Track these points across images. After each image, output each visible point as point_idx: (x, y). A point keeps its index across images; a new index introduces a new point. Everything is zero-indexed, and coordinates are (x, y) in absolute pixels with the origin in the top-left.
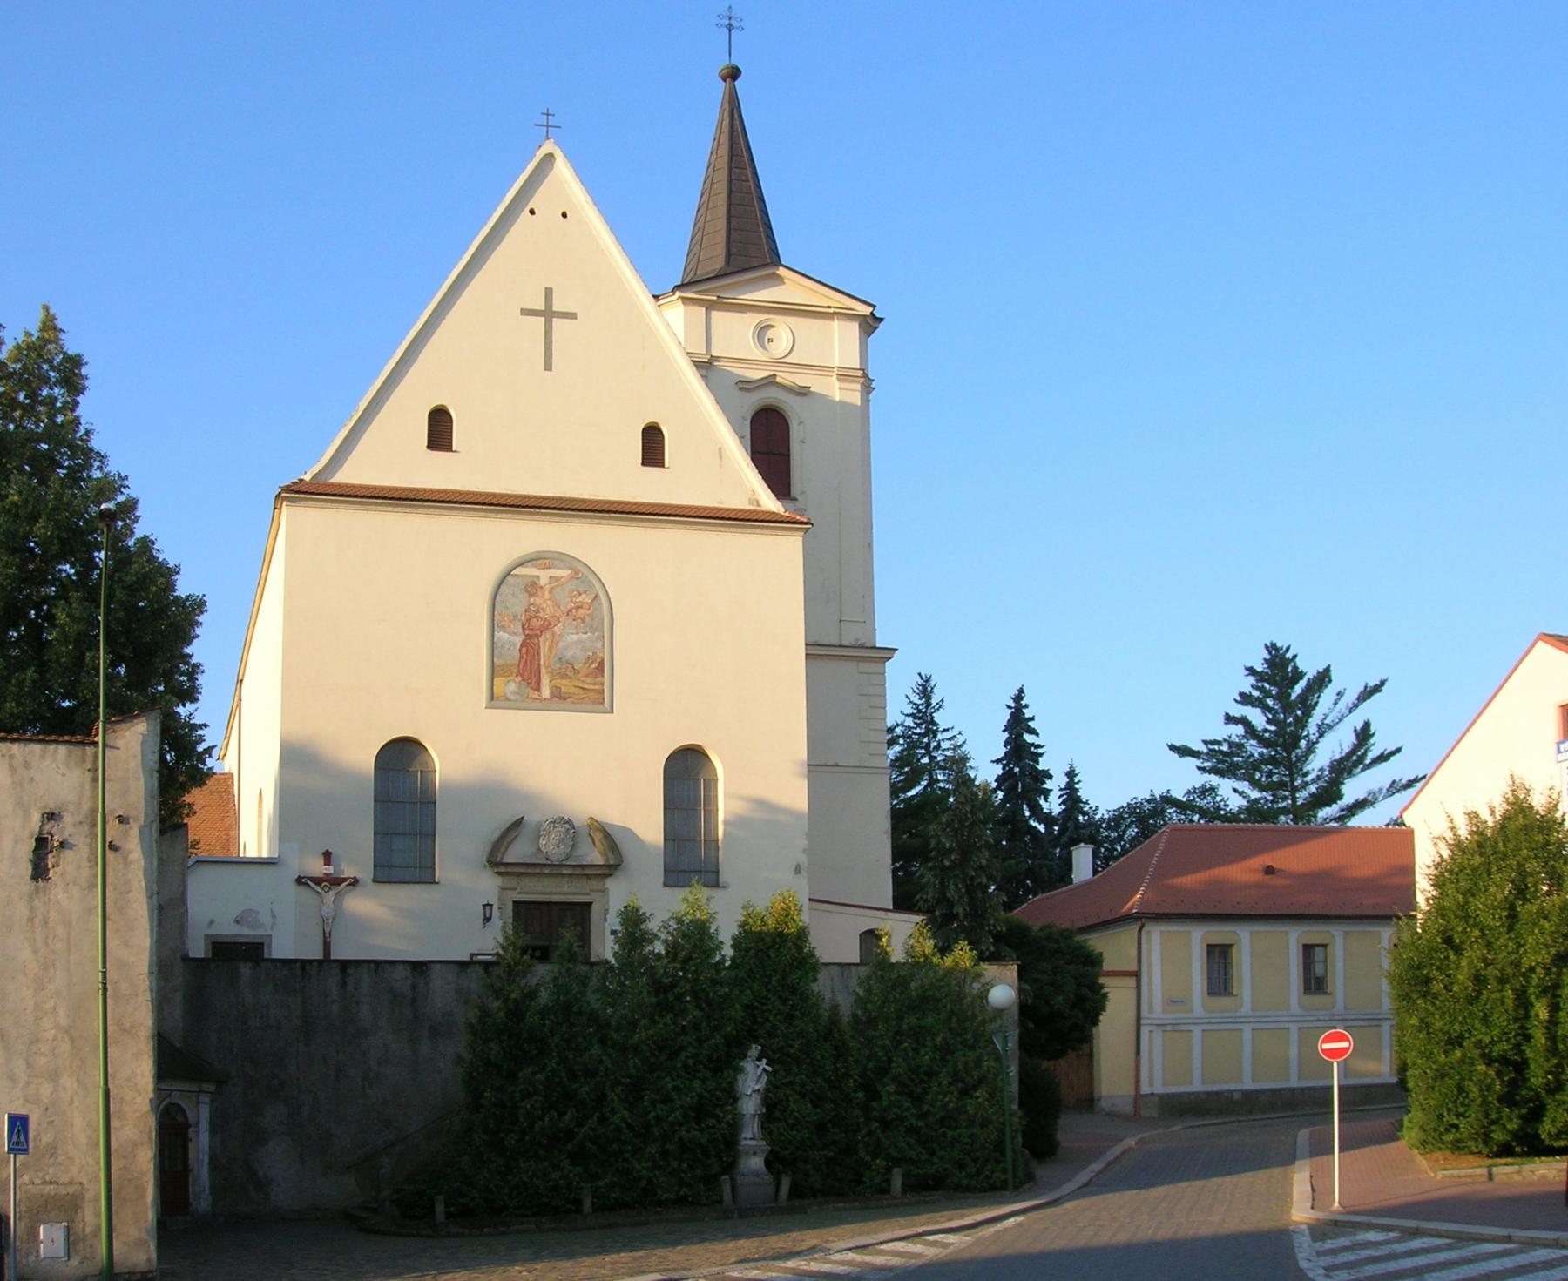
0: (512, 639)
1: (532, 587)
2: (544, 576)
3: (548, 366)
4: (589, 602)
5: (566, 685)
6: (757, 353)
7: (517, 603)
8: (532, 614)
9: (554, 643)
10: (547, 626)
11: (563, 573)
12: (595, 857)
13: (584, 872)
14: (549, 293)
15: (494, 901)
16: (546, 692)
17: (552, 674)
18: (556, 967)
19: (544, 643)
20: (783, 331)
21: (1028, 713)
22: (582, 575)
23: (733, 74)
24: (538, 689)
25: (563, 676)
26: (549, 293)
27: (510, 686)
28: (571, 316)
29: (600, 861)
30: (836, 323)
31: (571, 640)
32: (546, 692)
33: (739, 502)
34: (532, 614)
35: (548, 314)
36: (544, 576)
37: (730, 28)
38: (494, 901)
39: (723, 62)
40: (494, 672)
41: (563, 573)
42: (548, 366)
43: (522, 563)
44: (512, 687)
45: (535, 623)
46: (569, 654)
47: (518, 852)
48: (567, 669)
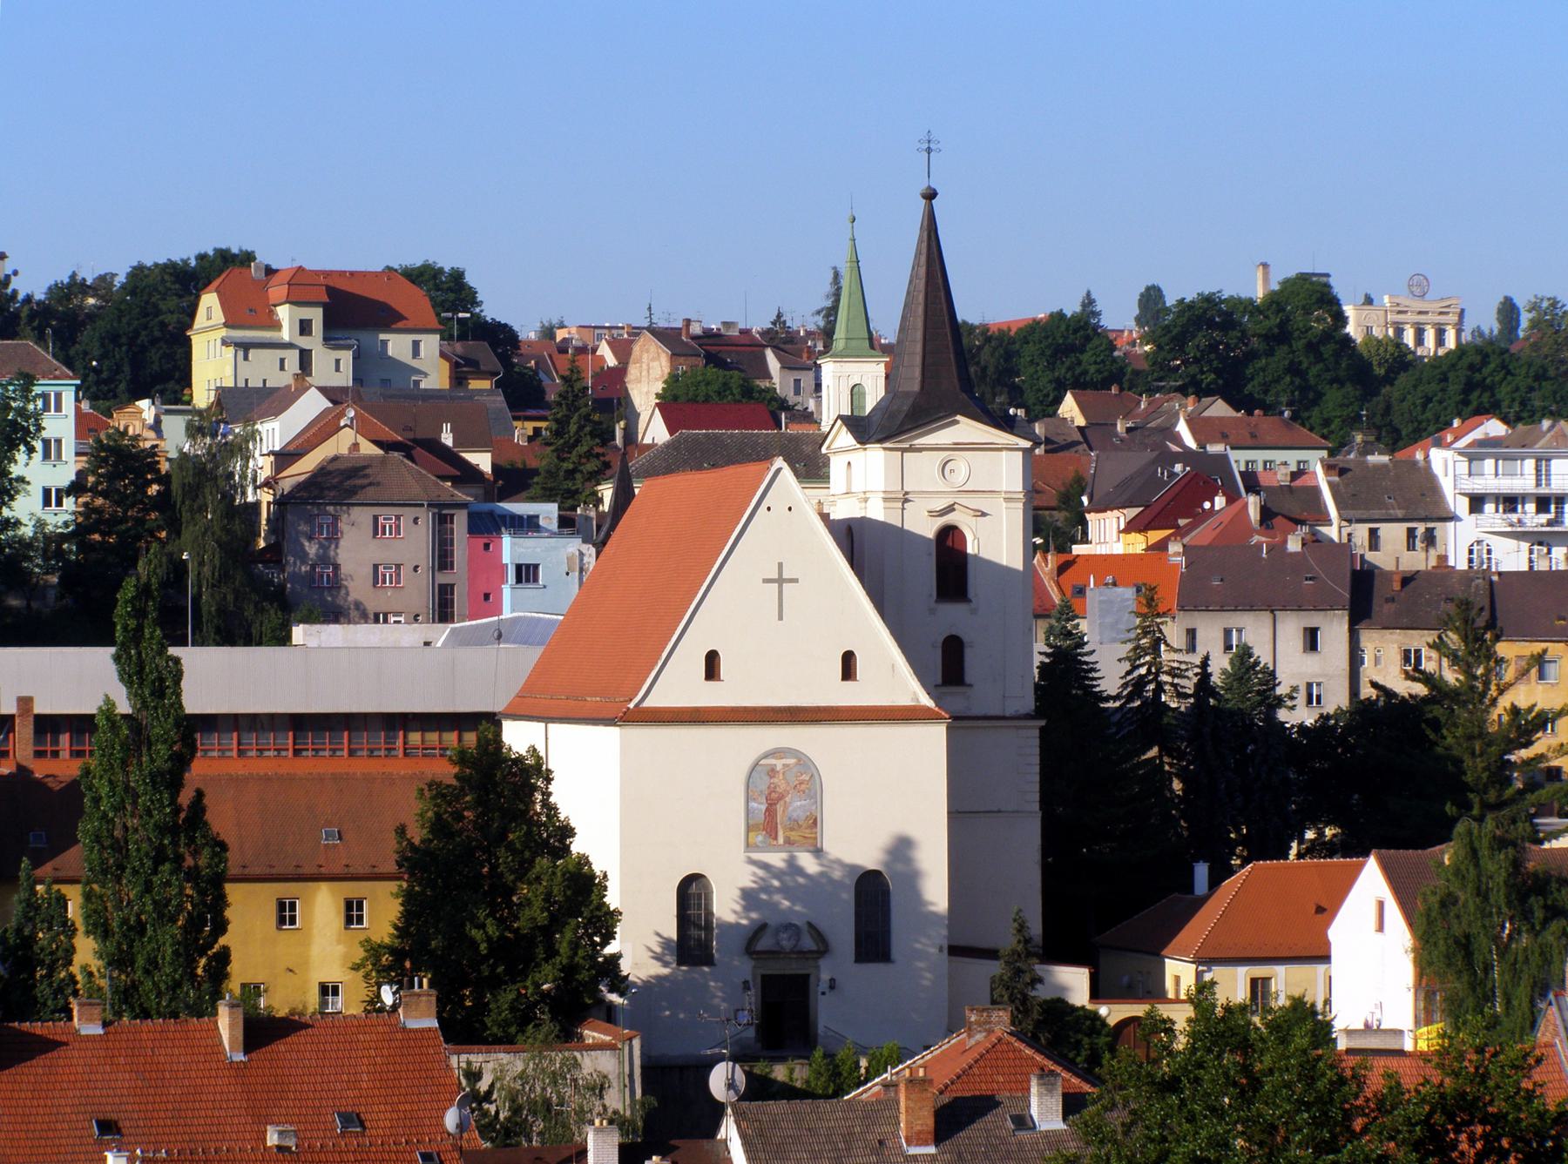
0: (760, 807)
1: (772, 772)
2: (779, 764)
3: (781, 618)
4: (807, 779)
5: (794, 835)
6: (941, 486)
7: (762, 783)
8: (772, 789)
9: (786, 808)
10: (781, 797)
11: (792, 761)
12: (808, 943)
13: (803, 955)
14: (766, 581)
15: (749, 978)
16: (781, 840)
17: (785, 829)
18: (1441, 1025)
19: (780, 808)
20: (962, 464)
21: (205, 801)
22: (803, 762)
23: (930, 195)
24: (776, 838)
25: (792, 829)
26: (766, 581)
27: (759, 838)
28: (795, 581)
29: (814, 948)
30: (1004, 453)
31: (796, 806)
32: (781, 840)
33: (904, 700)
34: (772, 789)
35: (780, 581)
36: (779, 764)
37: (929, 150)
38: (749, 978)
39: (922, 186)
40: (749, 829)
41: (792, 761)
42: (781, 618)
43: (766, 756)
44: (760, 838)
45: (774, 795)
46: (795, 815)
47: (764, 943)
48: (794, 825)
